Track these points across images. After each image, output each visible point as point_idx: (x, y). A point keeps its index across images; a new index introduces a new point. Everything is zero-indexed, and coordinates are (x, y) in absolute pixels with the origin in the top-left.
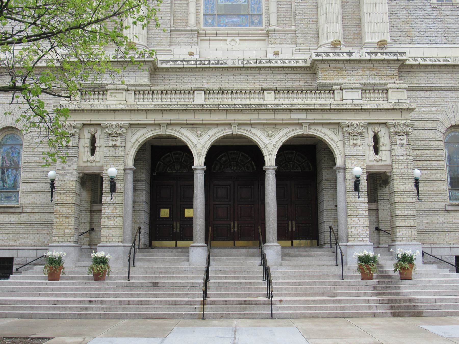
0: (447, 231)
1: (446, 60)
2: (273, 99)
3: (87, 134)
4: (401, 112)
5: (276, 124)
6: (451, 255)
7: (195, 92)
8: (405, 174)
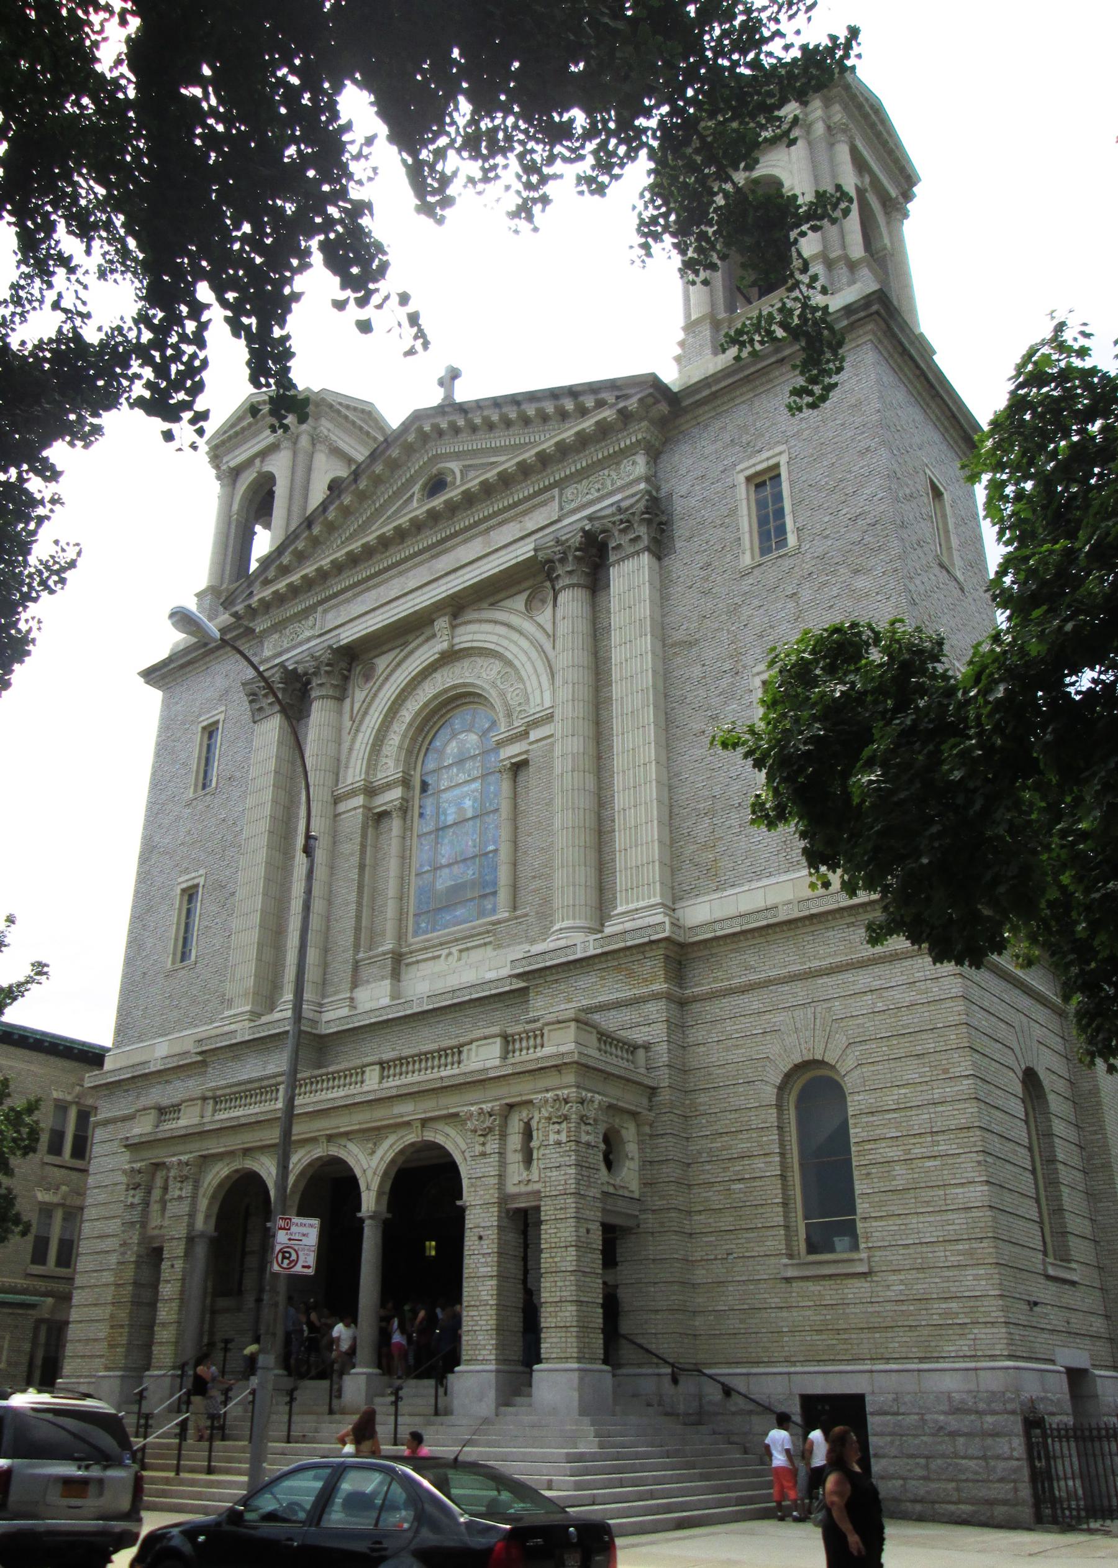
0: (785, 1329)
1: (769, 914)
2: (377, 1080)
3: (515, 1126)
4: (559, 1071)
5: (378, 1129)
6: (791, 1394)
7: (545, 1031)
8: (561, 1209)
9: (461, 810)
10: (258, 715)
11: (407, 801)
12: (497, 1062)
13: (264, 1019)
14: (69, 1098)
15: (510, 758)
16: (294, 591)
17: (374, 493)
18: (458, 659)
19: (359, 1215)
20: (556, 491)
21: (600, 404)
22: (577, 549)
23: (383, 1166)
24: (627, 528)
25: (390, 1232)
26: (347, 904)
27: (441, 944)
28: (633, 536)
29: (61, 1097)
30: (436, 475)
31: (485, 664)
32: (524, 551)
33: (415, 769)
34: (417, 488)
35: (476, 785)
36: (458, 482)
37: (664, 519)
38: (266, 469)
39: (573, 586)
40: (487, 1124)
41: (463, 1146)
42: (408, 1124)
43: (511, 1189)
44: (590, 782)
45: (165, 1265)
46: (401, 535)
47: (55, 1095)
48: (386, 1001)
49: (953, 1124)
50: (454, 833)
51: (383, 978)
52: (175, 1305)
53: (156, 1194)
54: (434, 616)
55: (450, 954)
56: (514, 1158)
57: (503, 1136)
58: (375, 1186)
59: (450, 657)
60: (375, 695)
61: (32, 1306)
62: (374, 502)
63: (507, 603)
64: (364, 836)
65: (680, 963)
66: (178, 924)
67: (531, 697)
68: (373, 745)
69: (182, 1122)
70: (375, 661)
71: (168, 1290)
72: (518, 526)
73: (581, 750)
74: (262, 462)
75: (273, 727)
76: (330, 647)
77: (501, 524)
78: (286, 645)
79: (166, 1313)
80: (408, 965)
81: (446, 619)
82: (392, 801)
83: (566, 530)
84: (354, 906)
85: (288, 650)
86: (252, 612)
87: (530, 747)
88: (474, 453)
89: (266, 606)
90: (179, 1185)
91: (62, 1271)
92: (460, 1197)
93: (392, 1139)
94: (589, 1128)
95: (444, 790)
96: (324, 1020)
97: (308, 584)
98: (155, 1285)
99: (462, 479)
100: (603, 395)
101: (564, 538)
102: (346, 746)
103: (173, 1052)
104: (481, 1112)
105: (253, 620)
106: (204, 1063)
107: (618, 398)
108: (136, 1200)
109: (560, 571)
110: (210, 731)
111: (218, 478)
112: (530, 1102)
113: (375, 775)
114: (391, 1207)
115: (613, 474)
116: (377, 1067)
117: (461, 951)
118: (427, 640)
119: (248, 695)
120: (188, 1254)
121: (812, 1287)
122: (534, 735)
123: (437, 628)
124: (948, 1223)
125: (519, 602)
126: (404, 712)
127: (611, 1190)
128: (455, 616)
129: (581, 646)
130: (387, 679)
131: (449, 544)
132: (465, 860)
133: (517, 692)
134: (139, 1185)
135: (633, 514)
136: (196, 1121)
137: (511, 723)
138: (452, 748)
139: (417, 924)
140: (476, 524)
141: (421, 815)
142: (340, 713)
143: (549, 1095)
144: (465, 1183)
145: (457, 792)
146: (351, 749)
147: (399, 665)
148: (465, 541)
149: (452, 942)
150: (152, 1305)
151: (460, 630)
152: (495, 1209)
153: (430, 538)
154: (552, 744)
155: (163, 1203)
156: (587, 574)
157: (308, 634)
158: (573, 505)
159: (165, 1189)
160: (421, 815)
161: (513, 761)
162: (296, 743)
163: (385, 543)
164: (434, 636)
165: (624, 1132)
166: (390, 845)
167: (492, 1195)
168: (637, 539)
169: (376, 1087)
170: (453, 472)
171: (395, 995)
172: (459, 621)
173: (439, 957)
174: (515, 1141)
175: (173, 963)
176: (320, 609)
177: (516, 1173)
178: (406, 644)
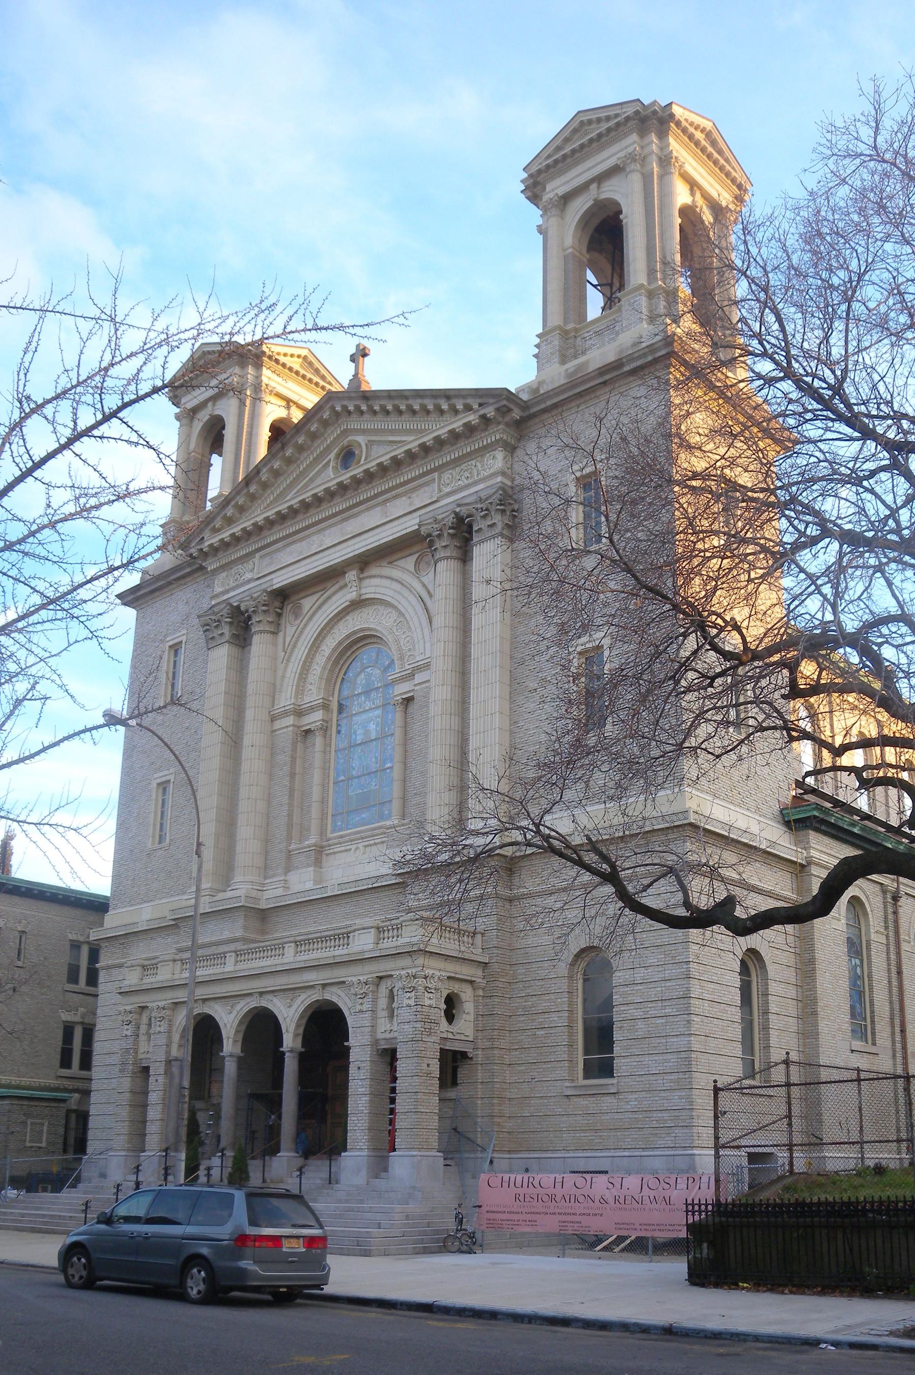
3: (383, 990)
9: (367, 732)
10: (211, 642)
11: (327, 722)
12: (371, 946)
13: (221, 896)
14: (82, 939)
15: (401, 694)
16: (236, 540)
17: (298, 459)
18: (365, 606)
19: (282, 1049)
20: (436, 475)
21: (468, 408)
22: (450, 528)
23: (297, 1016)
24: (485, 516)
25: (303, 1059)
26: (282, 805)
27: (351, 841)
28: (490, 523)
29: (75, 938)
30: (347, 447)
31: (386, 613)
32: (410, 525)
33: (333, 695)
34: (332, 456)
35: (378, 712)
36: (362, 462)
37: (516, 507)
38: (216, 413)
39: (447, 558)
40: (364, 990)
41: (350, 1005)
42: (312, 987)
43: (380, 1036)
44: (455, 722)
45: (152, 1079)
46: (318, 500)
47: (70, 937)
48: (309, 885)
49: (675, 994)
50: (362, 751)
51: (309, 865)
52: (160, 1107)
53: (143, 1028)
54: (345, 570)
55: (357, 848)
56: (383, 1014)
57: (375, 1001)
58: (292, 1028)
59: (357, 604)
60: (302, 632)
61: (64, 1101)
62: (299, 466)
63: (401, 563)
64: (294, 750)
65: (510, 870)
66: (156, 813)
67: (417, 645)
68: (301, 674)
69: (159, 978)
70: (302, 601)
71: (154, 1097)
72: (408, 502)
73: (449, 697)
74: (214, 405)
75: (222, 655)
76: (265, 591)
77: (396, 497)
78: (232, 584)
79: (154, 1113)
80: (327, 855)
81: (354, 572)
82: (315, 722)
83: (441, 511)
84: (286, 807)
85: (234, 589)
86: (204, 555)
87: (416, 688)
88: (376, 432)
89: (215, 550)
90: (158, 1023)
91: (84, 1073)
92: (348, 1040)
93: (303, 996)
94: (431, 995)
95: (355, 714)
96: (265, 897)
97: (247, 534)
98: (146, 1093)
99: (366, 459)
100: (469, 401)
101: (440, 517)
102: (280, 673)
103: (154, 917)
104: (360, 982)
105: (205, 560)
106: (176, 926)
107: (480, 405)
108: (129, 1033)
109: (438, 545)
110: (175, 649)
111: (178, 417)
112: (391, 976)
113: (302, 699)
114: (305, 1043)
115: (478, 464)
116: (293, 945)
117: (365, 846)
118: (341, 588)
119: (203, 626)
120: (168, 1072)
121: (583, 1102)
122: (419, 678)
123: (347, 580)
124: (666, 1061)
125: (409, 563)
126: (323, 647)
127: (450, 1036)
128: (362, 570)
129: (451, 611)
130: (310, 619)
131: (355, 510)
132: (369, 774)
133: (408, 639)
134: (131, 1022)
135: (491, 503)
136: (169, 976)
137: (402, 665)
138: (361, 679)
139: (334, 821)
140: (376, 496)
141: (339, 732)
142: (275, 644)
143: (403, 972)
144: (350, 1030)
145: (364, 716)
146: (283, 677)
147: (320, 607)
148: (368, 509)
149: (358, 839)
150: (144, 1106)
151: (366, 582)
152: (368, 1049)
153: (340, 504)
154: (429, 688)
155: (149, 1035)
156: (459, 548)
157: (249, 576)
158: (448, 489)
159: (150, 1025)
160: (339, 732)
161: (404, 697)
162: (240, 668)
163: (306, 506)
164: (346, 585)
165: (462, 995)
166: (314, 757)
167: (366, 1040)
168: (493, 525)
169: (292, 960)
170: (360, 446)
171: (318, 880)
172: (365, 574)
173: (350, 850)
174: (383, 1002)
175: (153, 844)
176: (258, 555)
177: (383, 1025)
178: (325, 589)
